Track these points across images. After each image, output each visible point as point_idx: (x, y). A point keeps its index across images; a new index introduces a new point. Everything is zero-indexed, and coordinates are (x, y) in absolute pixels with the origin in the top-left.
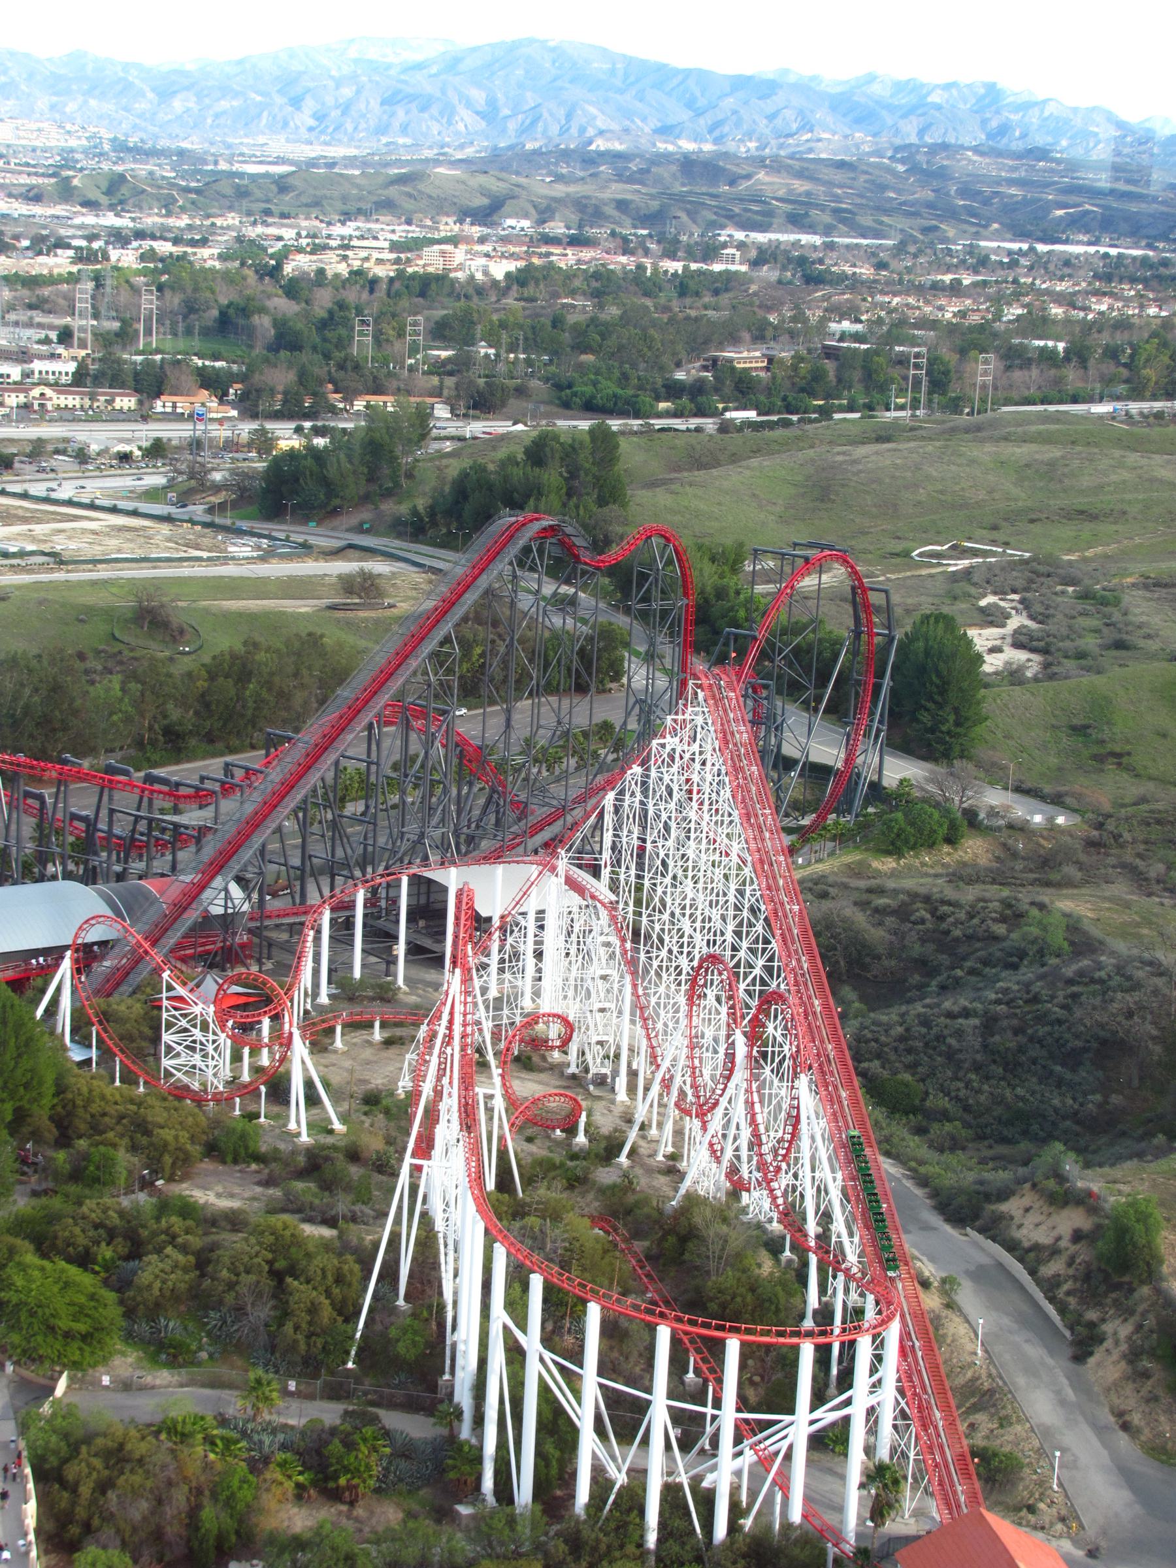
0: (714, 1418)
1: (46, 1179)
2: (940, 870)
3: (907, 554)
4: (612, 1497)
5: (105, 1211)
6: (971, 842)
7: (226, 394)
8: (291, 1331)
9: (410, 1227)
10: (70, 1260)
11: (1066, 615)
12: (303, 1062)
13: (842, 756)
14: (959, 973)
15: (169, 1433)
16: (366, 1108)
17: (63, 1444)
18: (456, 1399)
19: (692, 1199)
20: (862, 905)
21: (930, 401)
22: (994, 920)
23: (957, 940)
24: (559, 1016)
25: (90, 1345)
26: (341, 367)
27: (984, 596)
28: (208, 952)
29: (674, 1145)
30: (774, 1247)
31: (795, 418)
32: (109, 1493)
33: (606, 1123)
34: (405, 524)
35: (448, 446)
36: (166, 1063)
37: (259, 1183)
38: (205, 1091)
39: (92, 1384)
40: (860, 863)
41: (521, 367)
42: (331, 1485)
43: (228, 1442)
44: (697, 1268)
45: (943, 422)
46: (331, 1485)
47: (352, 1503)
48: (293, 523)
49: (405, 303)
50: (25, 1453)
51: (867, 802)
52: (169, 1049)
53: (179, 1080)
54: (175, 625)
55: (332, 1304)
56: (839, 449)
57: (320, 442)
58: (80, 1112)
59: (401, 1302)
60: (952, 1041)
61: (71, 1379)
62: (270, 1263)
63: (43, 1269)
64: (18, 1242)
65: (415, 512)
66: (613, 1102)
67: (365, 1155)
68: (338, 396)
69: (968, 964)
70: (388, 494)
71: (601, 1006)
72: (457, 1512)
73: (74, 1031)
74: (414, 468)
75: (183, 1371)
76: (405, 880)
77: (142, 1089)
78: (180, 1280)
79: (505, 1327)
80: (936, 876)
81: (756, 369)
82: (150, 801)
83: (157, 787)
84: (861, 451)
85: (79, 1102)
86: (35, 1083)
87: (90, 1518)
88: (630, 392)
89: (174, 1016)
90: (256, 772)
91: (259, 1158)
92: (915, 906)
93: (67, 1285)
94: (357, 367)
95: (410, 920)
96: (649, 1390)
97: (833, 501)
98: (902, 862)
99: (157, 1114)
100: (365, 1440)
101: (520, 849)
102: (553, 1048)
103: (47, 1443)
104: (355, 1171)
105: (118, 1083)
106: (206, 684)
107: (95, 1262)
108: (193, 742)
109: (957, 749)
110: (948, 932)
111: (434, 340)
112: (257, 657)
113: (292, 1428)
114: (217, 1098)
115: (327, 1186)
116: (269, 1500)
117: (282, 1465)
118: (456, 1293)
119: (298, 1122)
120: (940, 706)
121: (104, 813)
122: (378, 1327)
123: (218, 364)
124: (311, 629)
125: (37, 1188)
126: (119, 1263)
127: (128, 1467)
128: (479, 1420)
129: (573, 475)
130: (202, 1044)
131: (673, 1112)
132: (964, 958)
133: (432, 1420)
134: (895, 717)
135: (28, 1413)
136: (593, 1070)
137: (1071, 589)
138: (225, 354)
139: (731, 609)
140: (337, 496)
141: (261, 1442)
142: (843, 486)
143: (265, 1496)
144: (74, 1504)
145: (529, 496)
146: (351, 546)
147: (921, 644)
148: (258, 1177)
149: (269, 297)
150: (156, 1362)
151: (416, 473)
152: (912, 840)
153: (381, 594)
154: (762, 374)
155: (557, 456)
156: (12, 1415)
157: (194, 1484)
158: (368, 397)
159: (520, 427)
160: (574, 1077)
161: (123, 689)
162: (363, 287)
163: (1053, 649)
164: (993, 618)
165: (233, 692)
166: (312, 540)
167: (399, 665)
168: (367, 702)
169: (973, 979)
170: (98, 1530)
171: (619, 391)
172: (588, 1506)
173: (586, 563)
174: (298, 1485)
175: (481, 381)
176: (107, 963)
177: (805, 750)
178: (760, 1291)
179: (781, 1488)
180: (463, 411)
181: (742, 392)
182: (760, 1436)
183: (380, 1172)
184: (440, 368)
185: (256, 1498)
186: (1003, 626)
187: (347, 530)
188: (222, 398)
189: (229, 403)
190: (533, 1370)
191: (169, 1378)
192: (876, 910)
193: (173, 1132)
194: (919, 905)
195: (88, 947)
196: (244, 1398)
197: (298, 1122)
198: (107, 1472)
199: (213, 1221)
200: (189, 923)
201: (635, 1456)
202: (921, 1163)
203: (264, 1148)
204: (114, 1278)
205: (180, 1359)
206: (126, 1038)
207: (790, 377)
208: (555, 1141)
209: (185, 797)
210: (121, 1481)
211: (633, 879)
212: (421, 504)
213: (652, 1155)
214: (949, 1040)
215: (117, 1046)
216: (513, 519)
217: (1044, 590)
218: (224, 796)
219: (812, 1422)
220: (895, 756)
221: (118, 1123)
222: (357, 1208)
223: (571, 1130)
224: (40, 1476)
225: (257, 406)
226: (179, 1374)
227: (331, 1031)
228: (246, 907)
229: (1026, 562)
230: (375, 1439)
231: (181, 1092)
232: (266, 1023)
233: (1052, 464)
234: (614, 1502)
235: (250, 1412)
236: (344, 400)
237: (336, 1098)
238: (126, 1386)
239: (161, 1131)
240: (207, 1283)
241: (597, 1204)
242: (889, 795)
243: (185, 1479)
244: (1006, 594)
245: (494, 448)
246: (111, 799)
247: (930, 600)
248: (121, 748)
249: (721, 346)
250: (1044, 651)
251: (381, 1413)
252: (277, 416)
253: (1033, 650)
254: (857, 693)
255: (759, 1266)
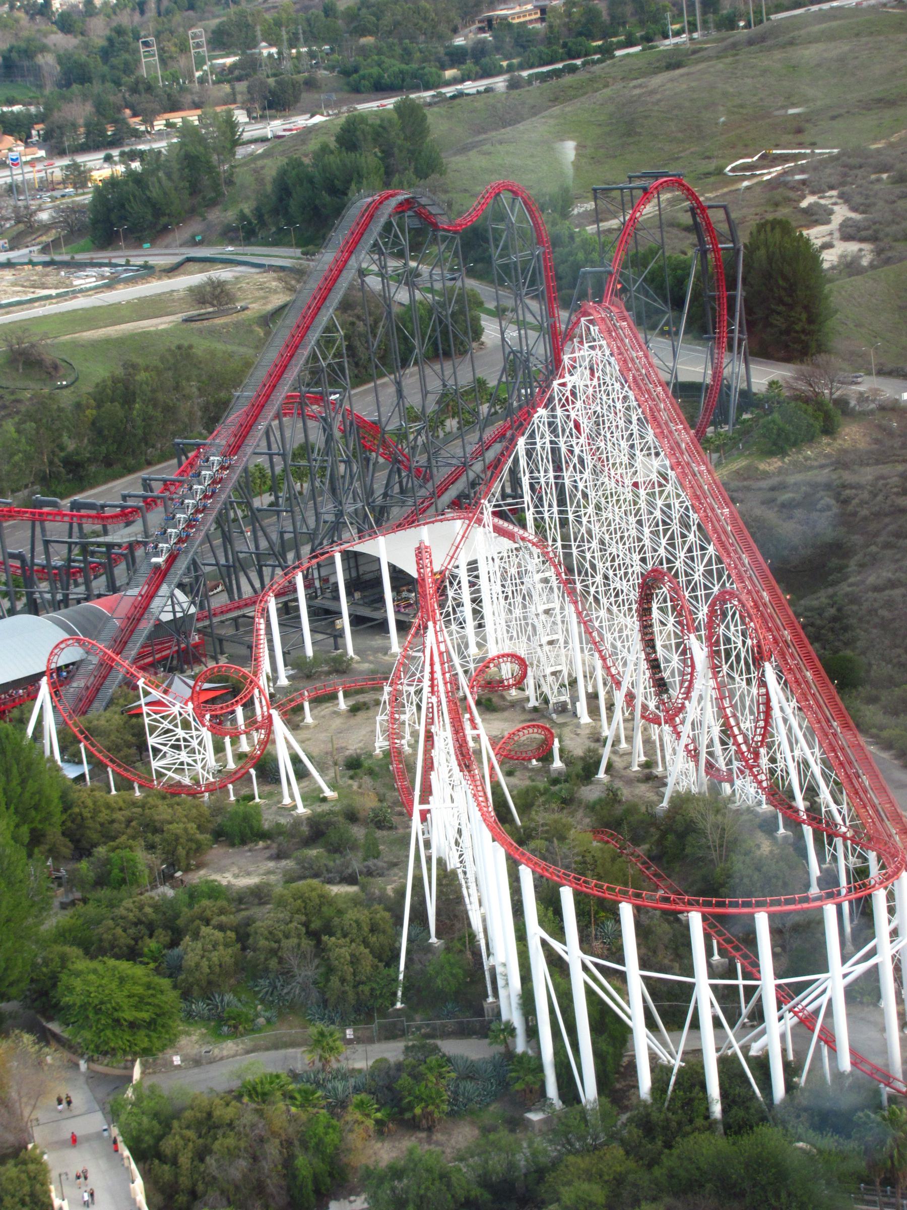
0: (750, 991)
1: (71, 891)
2: (823, 461)
3: (720, 171)
4: (673, 1079)
5: (141, 908)
6: (847, 430)
7: (29, 136)
8: (338, 983)
9: (429, 870)
10: (118, 957)
11: (886, 201)
12: (287, 742)
13: (710, 372)
14: (873, 549)
15: (250, 1096)
16: (351, 772)
17: (155, 1122)
18: (505, 1017)
19: (681, 801)
20: (768, 502)
21: (705, 22)
22: (897, 494)
23: (865, 519)
24: (508, 655)
25: (155, 1030)
26: (134, 90)
27: (803, 197)
28: (165, 658)
29: (646, 754)
30: (769, 826)
31: (578, 62)
32: (208, 1158)
33: (578, 748)
34: (236, 230)
35: (260, 149)
36: (155, 764)
37: (271, 858)
38: (197, 783)
39: (164, 1065)
40: (748, 468)
41: (305, 60)
42: (408, 1115)
43: (306, 1094)
44: (699, 859)
45: (724, 39)
46: (408, 1115)
47: (430, 1129)
48: (128, 247)
49: (178, 18)
50: (120, 1139)
51: (741, 409)
52: (156, 751)
53: (171, 778)
54: (48, 362)
55: (372, 952)
56: (635, 83)
57: (136, 165)
58: (90, 823)
59: (433, 939)
60: (884, 613)
61: (144, 1066)
62: (306, 925)
63: (95, 971)
64: (67, 949)
65: (242, 217)
66: (578, 726)
67: (362, 815)
68: (137, 120)
69: (881, 539)
70: (212, 203)
71: (550, 638)
72: (529, 1120)
73: (63, 750)
74: (232, 175)
75: (246, 1039)
76: (338, 557)
77: (138, 794)
78: (225, 955)
79: (544, 943)
80: (822, 467)
81: (531, 22)
82: (80, 526)
83: (83, 512)
84: (656, 81)
85: (87, 814)
86: (43, 804)
87: (195, 1185)
88: (415, 66)
89: (155, 720)
90: (173, 482)
91: (263, 835)
92: (819, 495)
93: (122, 980)
94: (149, 88)
95: (349, 594)
96: (691, 974)
97: (640, 134)
98: (786, 460)
99: (163, 812)
100: (430, 1069)
101: (432, 510)
102: (509, 687)
103: (140, 1124)
104: (358, 832)
105: (114, 792)
106: (94, 412)
107: (141, 955)
108: (93, 468)
109: (813, 345)
110: (855, 514)
111: (214, 50)
112: (138, 378)
113: (360, 1071)
114: (211, 789)
115: (336, 849)
116: (355, 1138)
117: (361, 1105)
118: (484, 920)
119: (292, 796)
120: (791, 307)
121: (39, 548)
122: (418, 967)
123: (16, 108)
124: (177, 342)
125: (65, 900)
126: (164, 952)
127: (220, 1132)
128: (532, 1032)
129: (387, 154)
130: (185, 740)
131: (639, 723)
132: (876, 535)
133: (487, 1041)
134: (750, 325)
135: (115, 1100)
136: (553, 700)
137: (885, 176)
138: (19, 97)
139: (570, 254)
140: (164, 215)
141: (334, 1088)
142: (646, 117)
143: (351, 1137)
144: (176, 1176)
145: (349, 182)
146: (189, 260)
147: (762, 252)
148: (267, 853)
149: (46, 35)
150: (220, 1035)
151: (235, 179)
152: (793, 438)
153: (232, 299)
154: (538, 26)
155: (369, 137)
156: (97, 1107)
157: (284, 1137)
158: (167, 116)
159: (318, 119)
160: (535, 709)
161: (18, 431)
162: (133, 9)
163: (881, 235)
164: (816, 216)
165: (121, 414)
166: (152, 261)
167: (292, 356)
168: (268, 396)
169: (889, 553)
170: (205, 1193)
171: (404, 67)
172: (654, 1090)
173: (444, 230)
174: (378, 1122)
175: (271, 81)
176: (75, 685)
177: (673, 372)
178: (764, 869)
179: (826, 1042)
180: (260, 113)
181: (522, 46)
182: (797, 999)
183: (379, 828)
184: (226, 75)
185: (342, 1140)
186: (828, 222)
187: (181, 246)
188: (26, 140)
189: (34, 144)
190: (578, 979)
191: (235, 1048)
192: (783, 506)
193: (181, 825)
194: (822, 493)
195: (59, 669)
196: (311, 1052)
197: (292, 796)
198: (201, 1141)
199: (243, 898)
200: (146, 632)
201: (687, 1040)
202: (881, 728)
203: (266, 826)
204: (164, 965)
205: (241, 1028)
206: (114, 748)
207: (565, 24)
208: (533, 770)
209: (112, 517)
210: (216, 1146)
211: (556, 515)
212: (247, 208)
213: (628, 766)
214: (882, 612)
215: (108, 757)
216: (370, 200)
217: (859, 182)
218: (148, 510)
219: (845, 976)
220: (760, 363)
221: (127, 826)
222: (370, 863)
223: (546, 757)
224: (139, 1156)
225: (62, 142)
226: (243, 1043)
227: (300, 708)
228: (193, 610)
229: (833, 158)
230: (440, 1066)
231: (176, 789)
232: (239, 711)
233: (842, 59)
234: (676, 1083)
235: (319, 1065)
236: (144, 122)
237: (321, 769)
238: (197, 1062)
239: (170, 826)
240: (250, 954)
241: (588, 820)
242: (760, 400)
243: (274, 1134)
244: (824, 191)
245: (304, 142)
246: (43, 530)
247: (753, 210)
248: (26, 486)
249: (492, 5)
250: (873, 239)
251: (439, 1042)
252: (84, 149)
253: (862, 240)
254: (713, 309)
255: (758, 846)
